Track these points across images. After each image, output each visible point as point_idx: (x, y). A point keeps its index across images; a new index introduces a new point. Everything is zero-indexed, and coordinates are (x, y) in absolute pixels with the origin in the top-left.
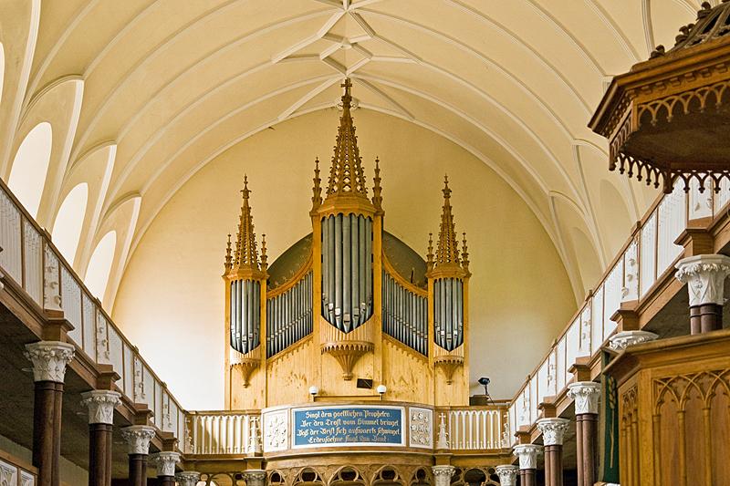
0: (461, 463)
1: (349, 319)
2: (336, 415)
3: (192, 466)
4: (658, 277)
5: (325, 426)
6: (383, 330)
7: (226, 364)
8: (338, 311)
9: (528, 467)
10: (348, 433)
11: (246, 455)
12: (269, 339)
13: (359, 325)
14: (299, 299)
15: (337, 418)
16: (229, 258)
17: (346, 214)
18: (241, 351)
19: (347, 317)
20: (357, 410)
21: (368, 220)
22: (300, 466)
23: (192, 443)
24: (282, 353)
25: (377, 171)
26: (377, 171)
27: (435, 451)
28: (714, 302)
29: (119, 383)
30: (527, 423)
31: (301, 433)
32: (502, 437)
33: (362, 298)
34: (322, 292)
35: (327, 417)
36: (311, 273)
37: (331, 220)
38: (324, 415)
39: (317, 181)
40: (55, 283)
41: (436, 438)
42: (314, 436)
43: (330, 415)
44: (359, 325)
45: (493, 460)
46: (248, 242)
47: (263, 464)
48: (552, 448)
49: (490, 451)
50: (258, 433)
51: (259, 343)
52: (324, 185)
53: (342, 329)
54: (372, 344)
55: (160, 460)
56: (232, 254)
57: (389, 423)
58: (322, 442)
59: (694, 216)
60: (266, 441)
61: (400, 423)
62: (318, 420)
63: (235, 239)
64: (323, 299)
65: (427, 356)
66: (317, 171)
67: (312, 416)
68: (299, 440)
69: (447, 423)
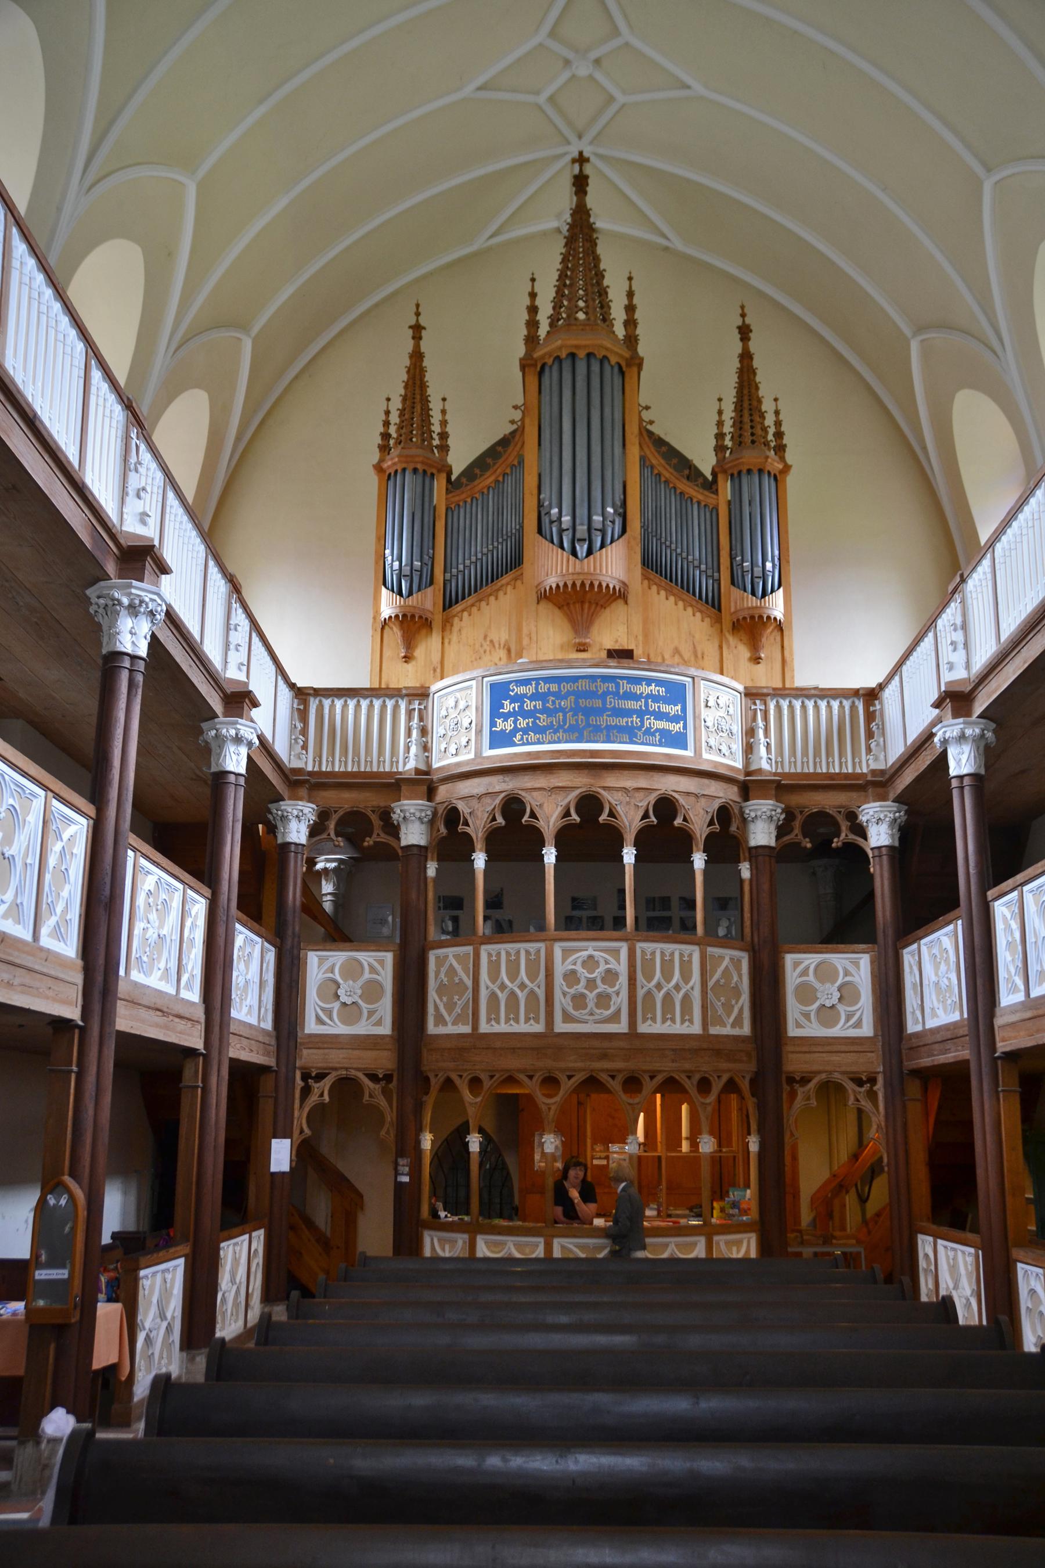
0: (797, 799)
1: (586, 536)
2: (566, 687)
3: (303, 792)
4: (1002, 640)
5: (545, 711)
6: (643, 564)
7: (374, 618)
8: (566, 519)
9: (965, 770)
10: (588, 725)
11: (400, 773)
12: (448, 576)
13: (603, 546)
14: (499, 511)
15: (569, 694)
16: (386, 436)
17: (582, 354)
18: (400, 593)
19: (582, 530)
20: (606, 678)
21: (616, 369)
22: (497, 789)
23: (305, 747)
24: (469, 600)
25: (630, 294)
26: (630, 294)
27: (748, 774)
28: (977, 771)
29: (255, 713)
30: (960, 674)
31: (501, 725)
32: (869, 750)
33: (609, 500)
34: (539, 493)
35: (549, 693)
36: (521, 462)
37: (555, 367)
38: (543, 688)
39: (533, 310)
40: (243, 665)
41: (749, 749)
42: (525, 731)
43: (554, 687)
44: (603, 546)
45: (854, 795)
46: (418, 408)
47: (430, 793)
48: (967, 781)
49: (847, 776)
50: (424, 731)
51: (431, 583)
52: (545, 310)
53: (574, 553)
54: (624, 583)
55: (217, 736)
56: (393, 430)
57: (665, 708)
58: (539, 742)
59: (947, 677)
60: (437, 746)
61: (684, 709)
62: (533, 697)
63: (396, 404)
64: (540, 505)
65: (720, 610)
66: (533, 295)
67: (521, 690)
68: (498, 739)
69: (766, 718)
